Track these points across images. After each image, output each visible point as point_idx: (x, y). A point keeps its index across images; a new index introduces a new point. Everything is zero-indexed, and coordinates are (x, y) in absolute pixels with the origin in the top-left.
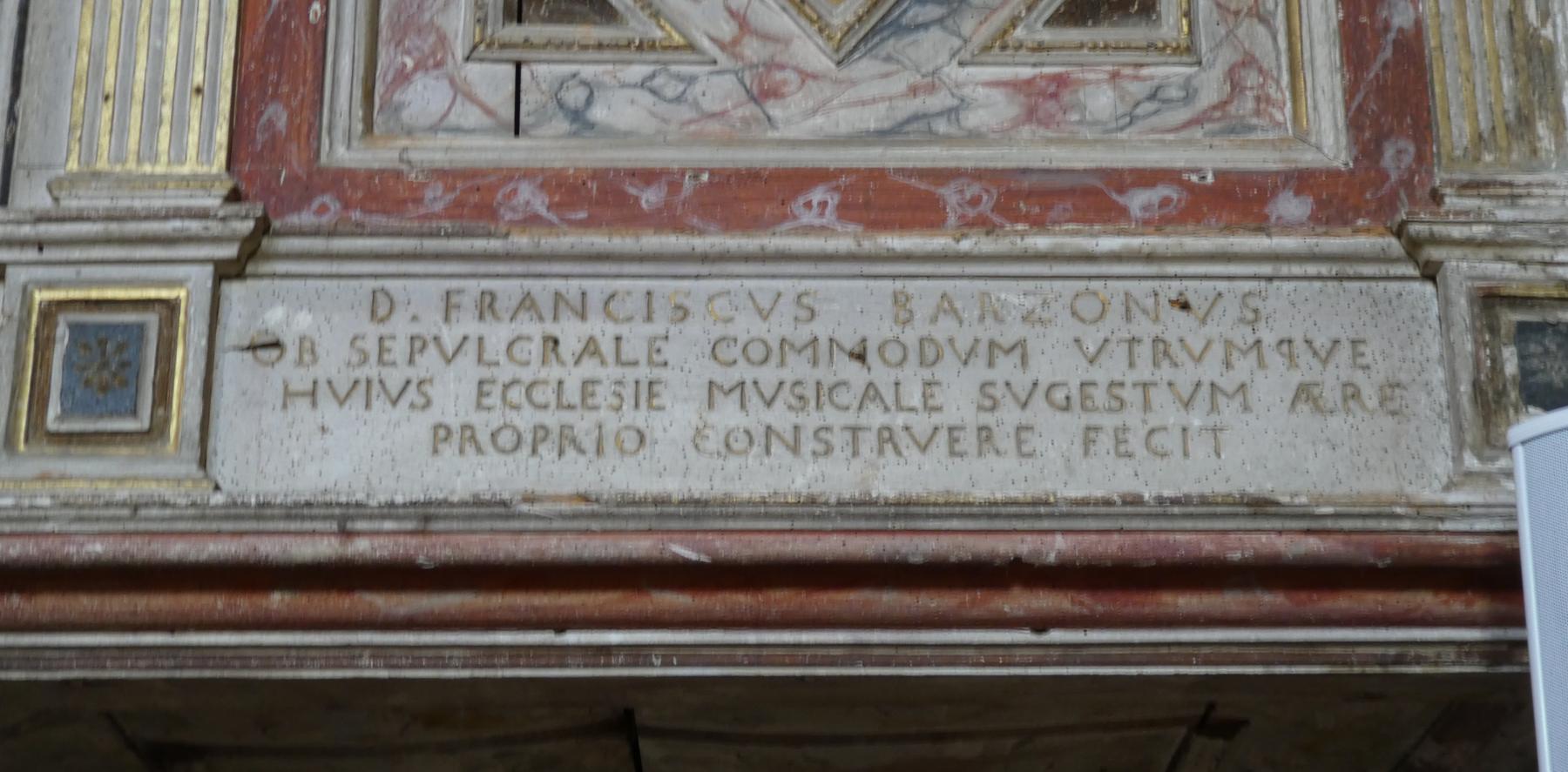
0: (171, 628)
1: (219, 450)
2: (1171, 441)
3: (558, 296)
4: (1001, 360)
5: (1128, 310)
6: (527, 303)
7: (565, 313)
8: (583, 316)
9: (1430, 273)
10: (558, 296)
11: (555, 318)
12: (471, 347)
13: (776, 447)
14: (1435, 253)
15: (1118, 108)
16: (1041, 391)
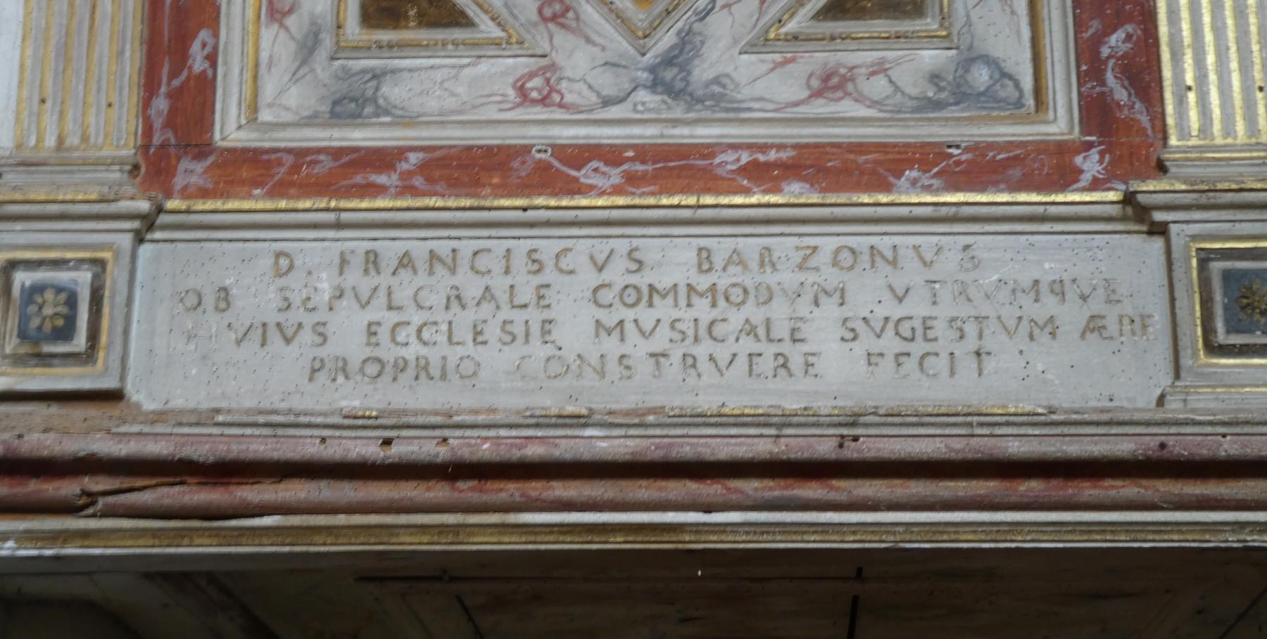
0: (708, 509)
1: (874, 404)
2: (942, 363)
3: (433, 256)
4: (696, 300)
5: (454, 259)
6: (406, 262)
7: (439, 269)
8: (453, 271)
9: (1159, 230)
10: (433, 256)
11: (431, 273)
12: (382, 293)
13: (595, 361)
14: (1159, 216)
15: (891, 74)
16: (891, 325)
